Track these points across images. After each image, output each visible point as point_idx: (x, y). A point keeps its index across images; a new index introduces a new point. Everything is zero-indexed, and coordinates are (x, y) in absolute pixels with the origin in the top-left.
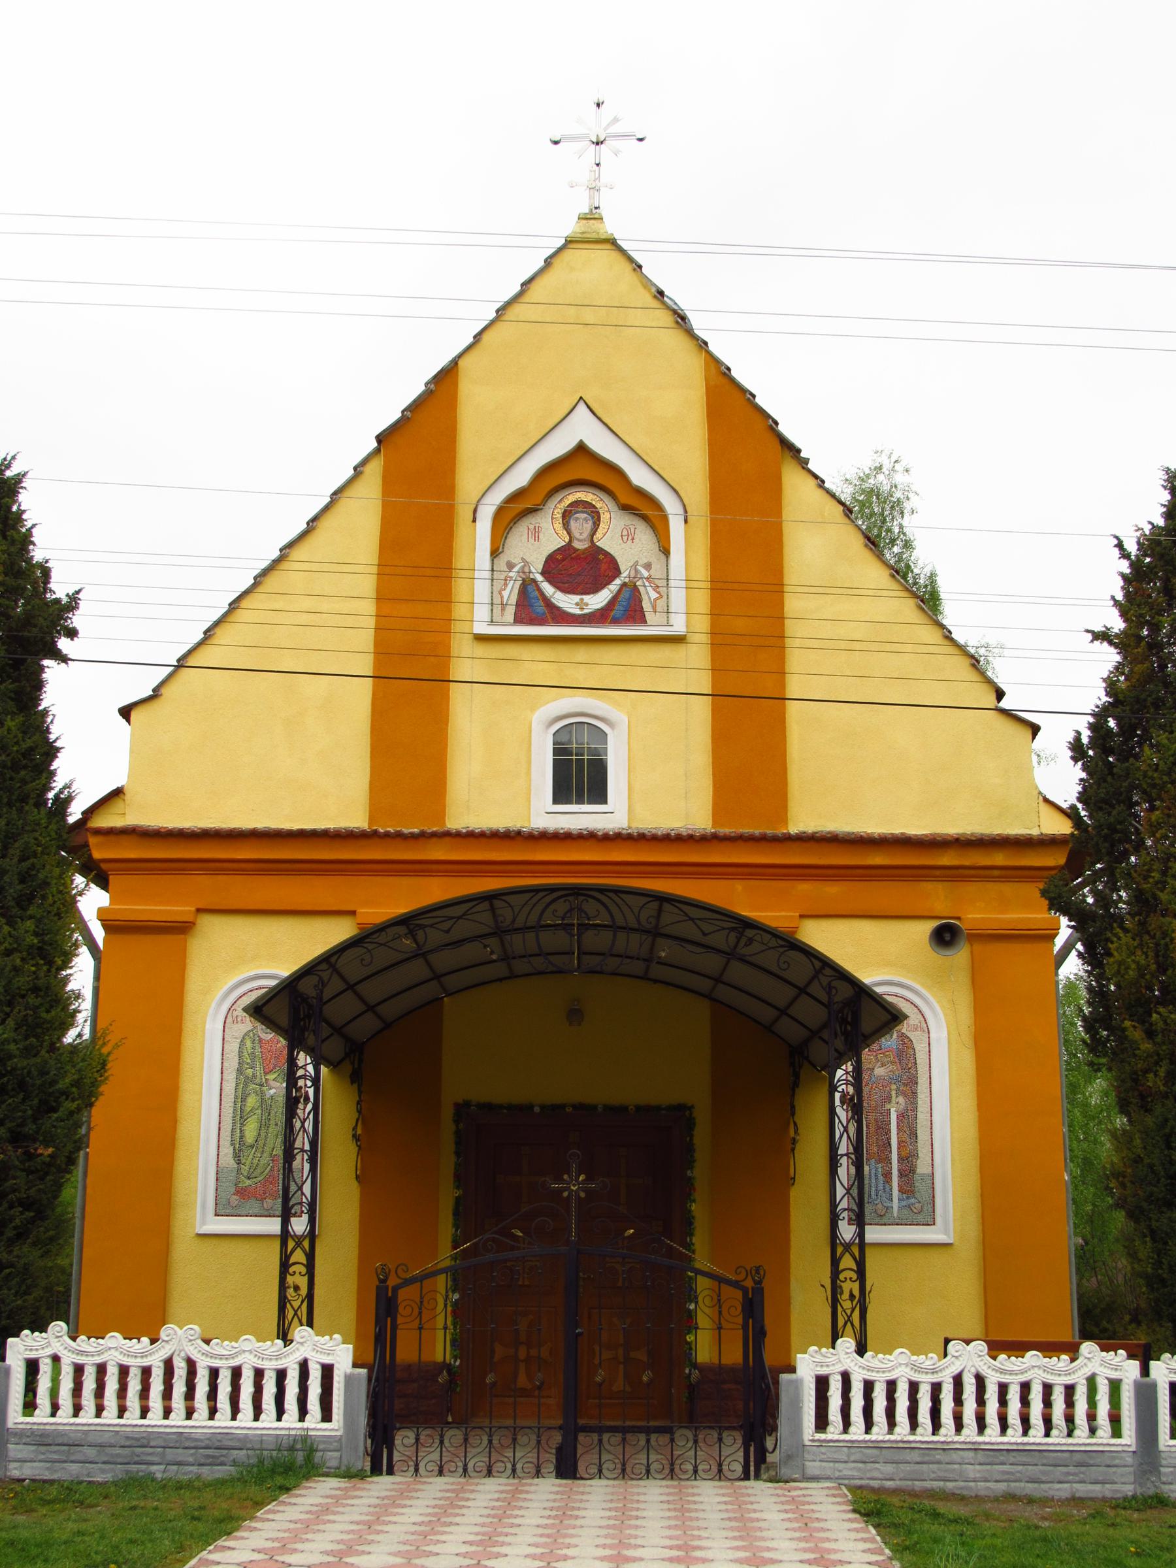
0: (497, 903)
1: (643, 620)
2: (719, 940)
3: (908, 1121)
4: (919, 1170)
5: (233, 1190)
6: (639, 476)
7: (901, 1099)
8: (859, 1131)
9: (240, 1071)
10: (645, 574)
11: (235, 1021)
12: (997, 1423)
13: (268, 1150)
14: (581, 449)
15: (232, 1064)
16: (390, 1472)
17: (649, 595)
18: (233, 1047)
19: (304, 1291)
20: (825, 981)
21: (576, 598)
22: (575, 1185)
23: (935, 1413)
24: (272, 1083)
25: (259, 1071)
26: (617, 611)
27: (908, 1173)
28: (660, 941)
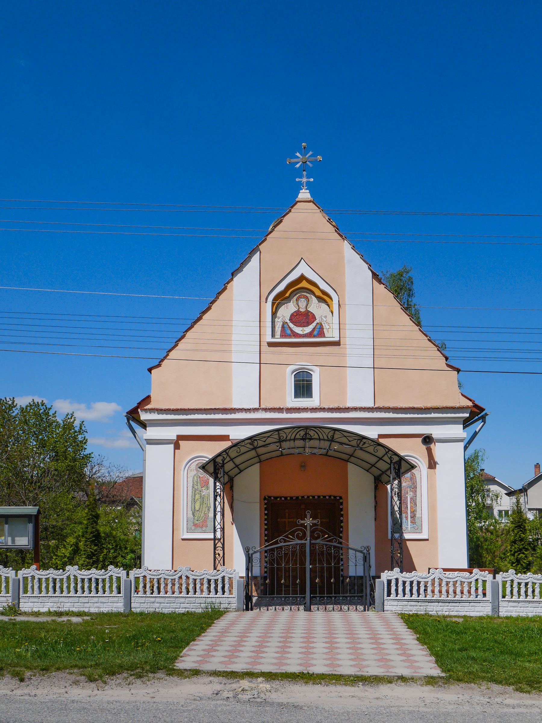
0: (280, 432)
1: (324, 336)
2: (354, 443)
3: (414, 500)
4: (417, 516)
5: (192, 524)
6: (323, 286)
7: (411, 493)
8: (400, 503)
9: (193, 487)
10: (325, 319)
11: (191, 471)
12: (402, 593)
13: (203, 512)
14: (302, 278)
15: (190, 485)
16: (252, 610)
17: (326, 326)
18: (190, 480)
19: (221, 555)
20: (389, 456)
21: (301, 328)
22: (308, 521)
23: (411, 590)
24: (204, 491)
25: (199, 487)
26: (315, 333)
27: (413, 517)
28: (333, 443)
